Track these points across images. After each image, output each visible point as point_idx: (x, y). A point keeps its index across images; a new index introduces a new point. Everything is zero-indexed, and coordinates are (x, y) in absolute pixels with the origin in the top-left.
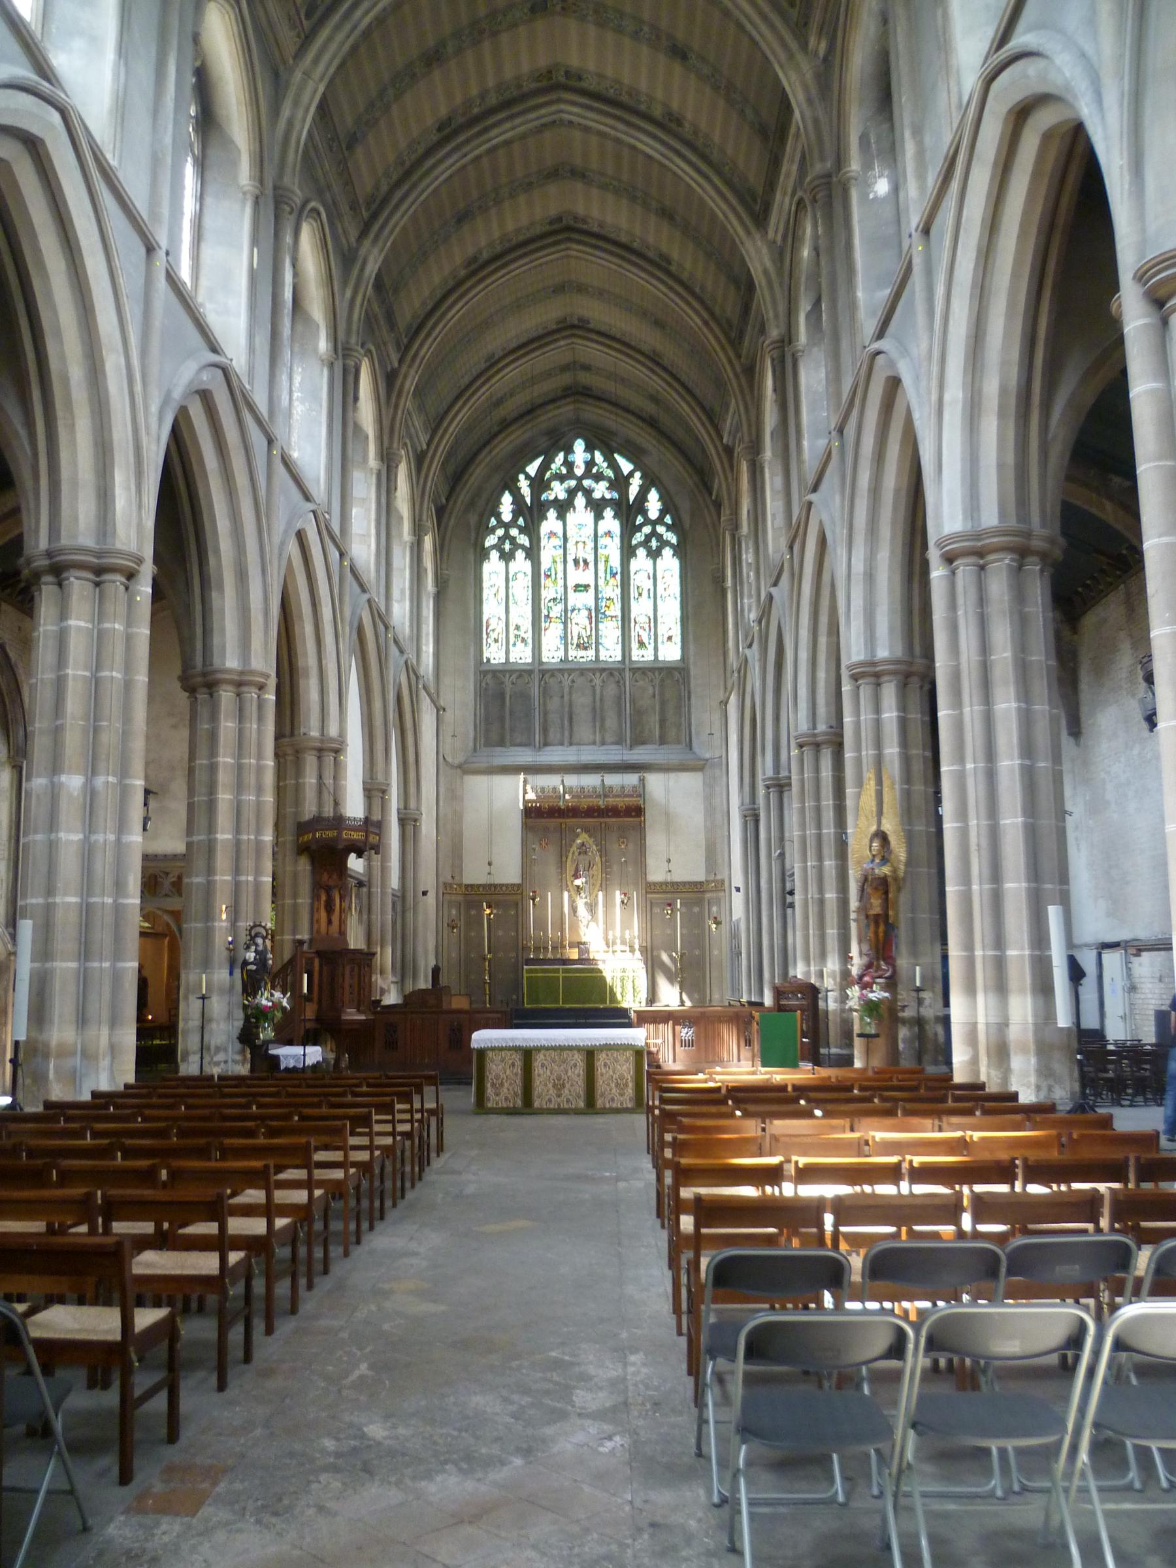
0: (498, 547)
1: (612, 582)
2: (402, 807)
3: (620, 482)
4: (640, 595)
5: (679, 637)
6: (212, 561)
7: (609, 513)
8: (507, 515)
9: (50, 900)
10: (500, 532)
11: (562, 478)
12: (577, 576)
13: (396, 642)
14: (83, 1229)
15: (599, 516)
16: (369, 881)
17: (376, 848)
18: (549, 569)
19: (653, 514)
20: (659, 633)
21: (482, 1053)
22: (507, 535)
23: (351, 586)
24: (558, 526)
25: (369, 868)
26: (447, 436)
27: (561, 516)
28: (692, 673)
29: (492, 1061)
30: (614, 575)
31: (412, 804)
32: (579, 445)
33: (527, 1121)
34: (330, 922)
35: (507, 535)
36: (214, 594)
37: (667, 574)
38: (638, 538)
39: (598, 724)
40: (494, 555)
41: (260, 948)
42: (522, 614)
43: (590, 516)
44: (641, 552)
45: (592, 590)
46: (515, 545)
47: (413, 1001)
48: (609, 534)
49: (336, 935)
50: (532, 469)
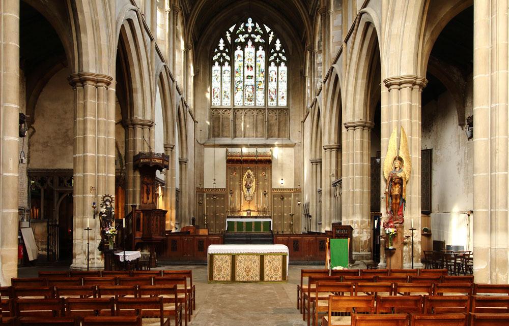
0: (218, 60)
1: (261, 75)
2: (180, 157)
3: (265, 36)
4: (272, 80)
5: (286, 97)
6: (80, 17)
7: (261, 48)
8: (221, 47)
10: (219, 54)
11: (243, 33)
12: (248, 73)
13: (177, 89)
14: (92, 297)
15: (257, 49)
17: (167, 167)
18: (238, 70)
19: (278, 49)
20: (279, 95)
21: (212, 256)
22: (221, 56)
23: (156, 58)
24: (241, 53)
26: (198, 8)
27: (243, 49)
28: (291, 111)
29: (217, 260)
30: (262, 72)
31: (185, 156)
32: (250, 20)
33: (233, 287)
34: (148, 198)
35: (221, 56)
36: (82, 35)
37: (283, 72)
38: (272, 58)
39: (255, 129)
40: (217, 63)
41: (109, 206)
42: (227, 86)
43: (253, 50)
44: (273, 64)
45: (254, 78)
46: (225, 60)
47: (184, 233)
48: (260, 56)
50: (232, 29)
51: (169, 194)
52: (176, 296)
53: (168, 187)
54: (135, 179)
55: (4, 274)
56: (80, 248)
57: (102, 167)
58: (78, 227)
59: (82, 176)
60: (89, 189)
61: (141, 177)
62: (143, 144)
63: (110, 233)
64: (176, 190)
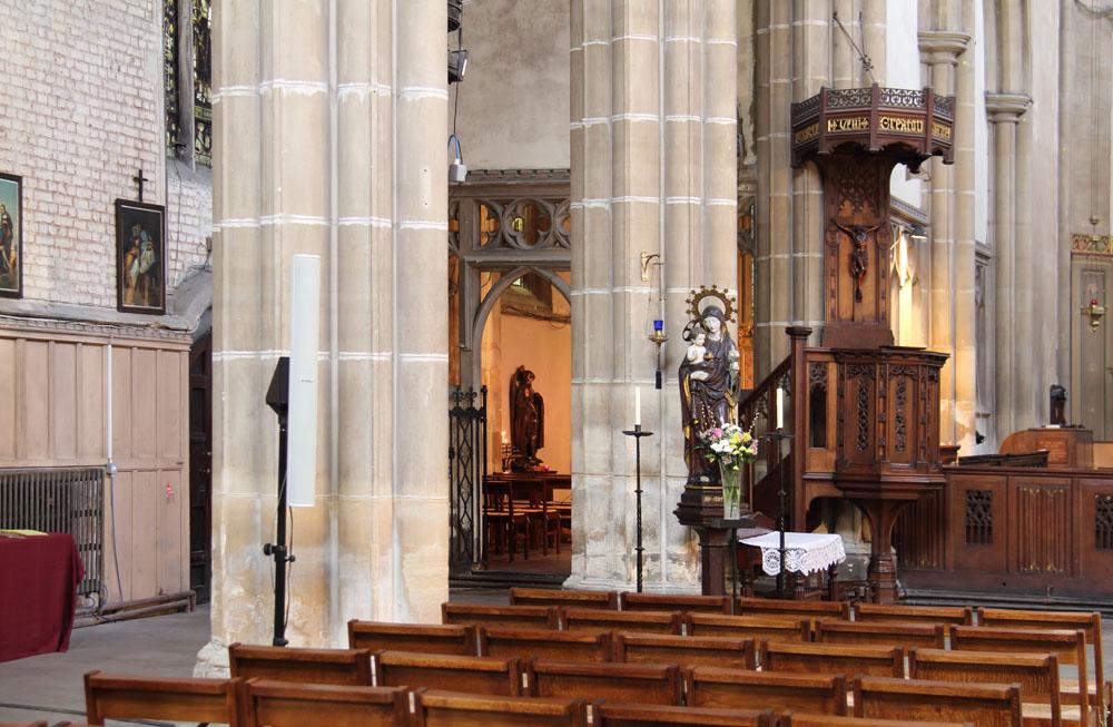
2: (993, 88)
9: (266, 221)
16: (932, 224)
17: (944, 151)
25: (932, 197)
31: (1014, 84)
34: (858, 297)
41: (717, 337)
47: (1019, 461)
49: (871, 322)
51: (944, 274)
52: (1056, 712)
53: (940, 241)
54: (802, 200)
55: (411, 590)
56: (601, 510)
57: (684, 171)
58: (593, 423)
59: (607, 207)
60: (634, 264)
61: (824, 198)
62: (835, 45)
63: (729, 449)
64: (978, 254)
